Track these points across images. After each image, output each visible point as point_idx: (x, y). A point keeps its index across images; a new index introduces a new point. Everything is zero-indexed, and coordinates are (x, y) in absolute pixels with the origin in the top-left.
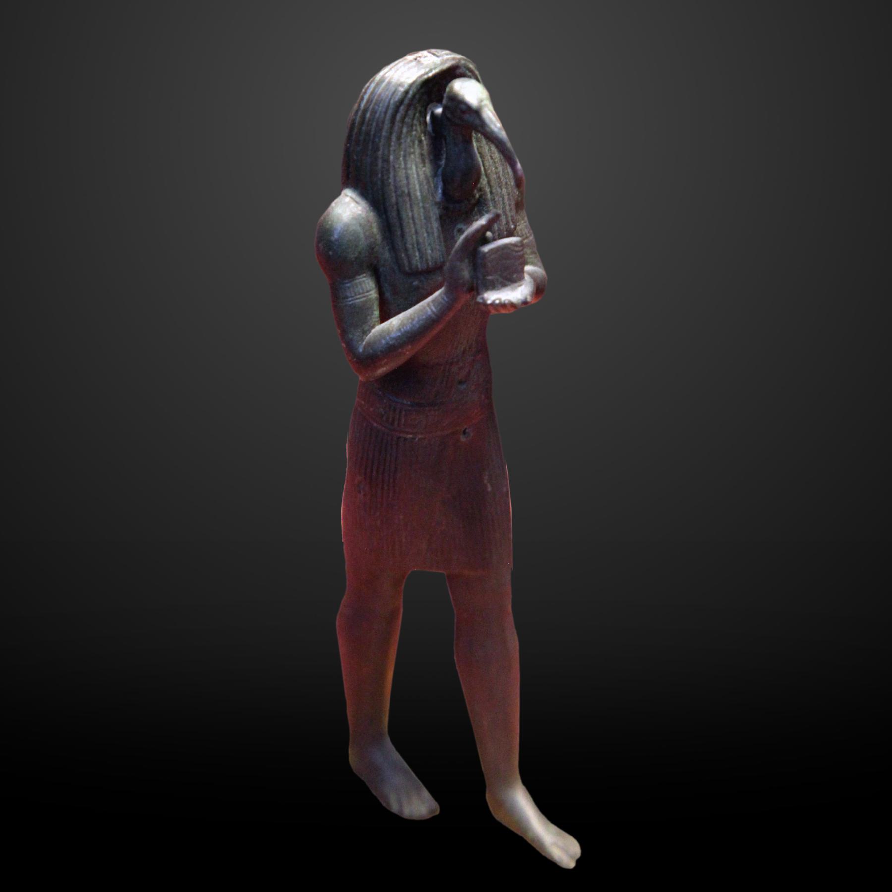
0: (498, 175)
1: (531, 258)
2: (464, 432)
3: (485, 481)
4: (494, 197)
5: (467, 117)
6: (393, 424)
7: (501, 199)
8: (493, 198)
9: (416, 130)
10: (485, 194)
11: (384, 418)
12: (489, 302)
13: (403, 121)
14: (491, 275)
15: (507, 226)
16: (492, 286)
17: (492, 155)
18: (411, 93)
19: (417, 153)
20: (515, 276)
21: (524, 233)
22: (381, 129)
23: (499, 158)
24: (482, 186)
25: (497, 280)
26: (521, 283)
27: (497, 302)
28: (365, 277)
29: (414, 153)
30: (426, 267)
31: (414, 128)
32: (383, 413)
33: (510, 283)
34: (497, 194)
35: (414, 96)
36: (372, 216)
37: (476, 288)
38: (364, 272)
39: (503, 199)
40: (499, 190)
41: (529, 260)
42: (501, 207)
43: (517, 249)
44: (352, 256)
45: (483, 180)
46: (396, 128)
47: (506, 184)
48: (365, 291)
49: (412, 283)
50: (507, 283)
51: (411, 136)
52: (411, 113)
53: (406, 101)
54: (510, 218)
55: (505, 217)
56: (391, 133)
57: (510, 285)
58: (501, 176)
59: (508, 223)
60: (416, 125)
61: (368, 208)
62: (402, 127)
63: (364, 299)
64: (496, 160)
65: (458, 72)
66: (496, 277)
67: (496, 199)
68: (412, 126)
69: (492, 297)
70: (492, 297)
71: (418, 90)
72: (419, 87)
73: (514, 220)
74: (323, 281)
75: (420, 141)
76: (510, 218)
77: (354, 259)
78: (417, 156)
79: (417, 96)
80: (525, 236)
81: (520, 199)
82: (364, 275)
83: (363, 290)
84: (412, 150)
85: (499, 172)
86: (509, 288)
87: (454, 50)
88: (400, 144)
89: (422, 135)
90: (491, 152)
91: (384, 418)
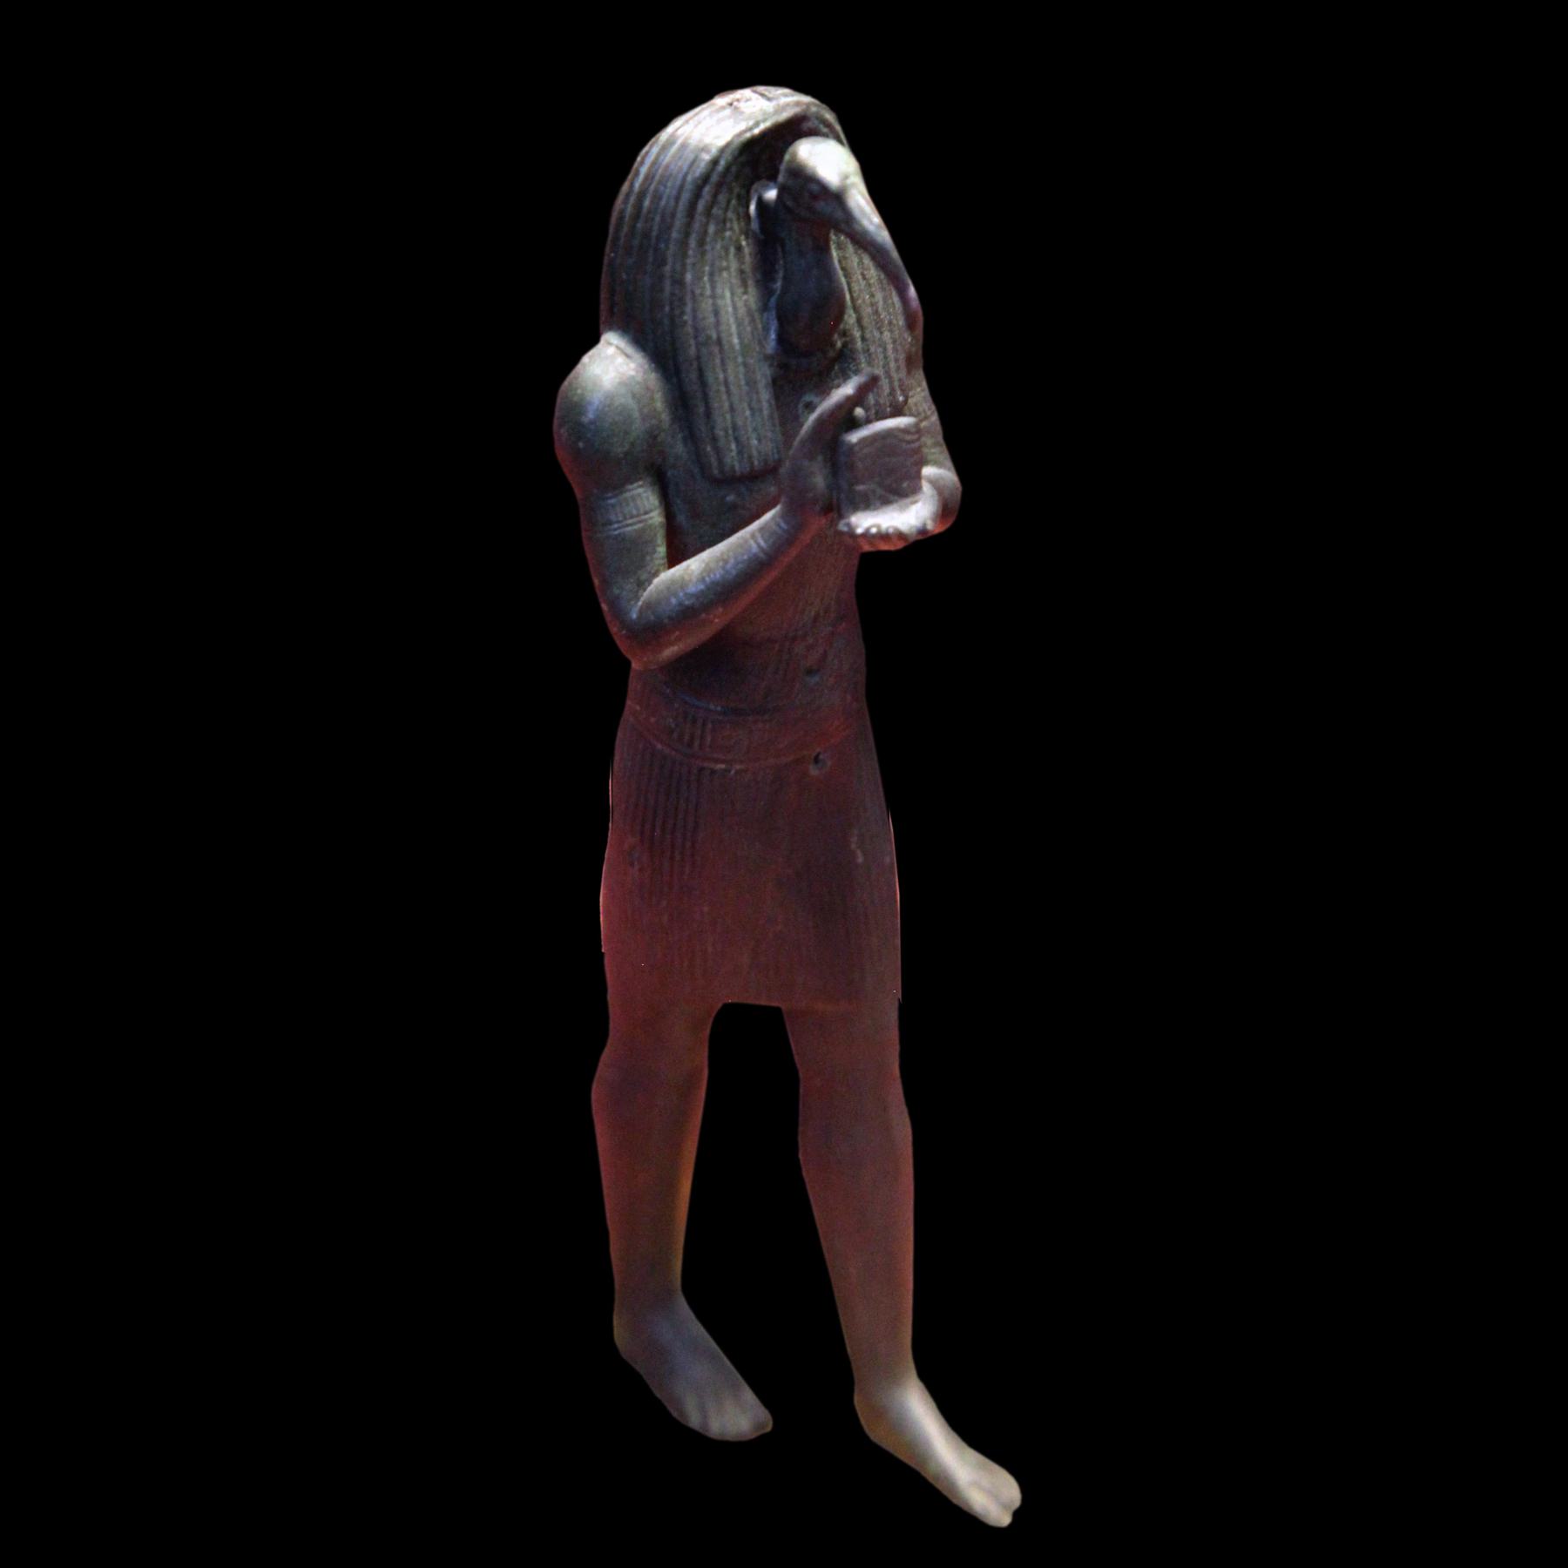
1: (934, 453)
2: (816, 760)
3: (853, 846)
4: (868, 345)
5: (820, 206)
6: (690, 745)
7: (880, 350)
8: (866, 348)
9: (731, 229)
10: (853, 340)
11: (675, 735)
13: (708, 213)
14: (863, 483)
15: (891, 398)
16: (865, 503)
17: (865, 272)
18: (722, 163)
19: (732, 269)
20: (905, 485)
21: (921, 409)
22: (670, 228)
23: (877, 278)
24: (847, 327)
25: (874, 492)
26: (916, 498)
27: (874, 530)
28: (641, 486)
29: (727, 269)
30: (748, 469)
31: (728, 225)
32: (673, 726)
33: (896, 498)
34: (874, 341)
35: (728, 169)
36: (653, 379)
38: (640, 479)
39: (885, 349)
40: (876, 334)
41: (930, 457)
42: (881, 363)
43: (908, 438)
44: (620, 450)
46: (696, 226)
47: (890, 323)
48: (642, 512)
49: (724, 497)
50: (891, 497)
51: (723, 239)
52: (722, 198)
53: (715, 178)
54: (896, 384)
55: (887, 381)
56: (687, 234)
57: (897, 501)
58: (880, 309)
59: (892, 392)
60: (731, 220)
61: (646, 366)
62: (707, 224)
64: (872, 281)
65: (806, 126)
66: (873, 486)
67: (872, 349)
68: (724, 221)
69: (865, 522)
70: (865, 522)
71: (735, 159)
72: (736, 153)
73: (903, 388)
75: (739, 249)
76: (896, 384)
77: (621, 455)
78: (734, 274)
79: (734, 169)
80: (923, 415)
82: (641, 483)
84: (725, 264)
85: (877, 303)
86: (895, 506)
89: (743, 237)
91: (675, 735)
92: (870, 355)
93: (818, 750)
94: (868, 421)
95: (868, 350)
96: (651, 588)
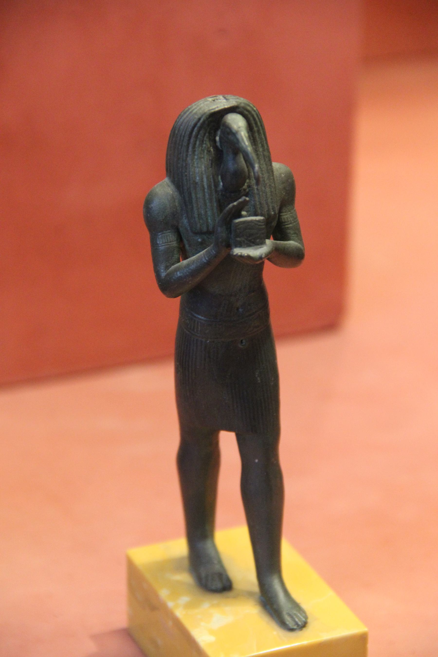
0: (263, 179)
1: (293, 237)
2: (242, 342)
3: (257, 376)
4: (259, 192)
5: (230, 137)
6: (193, 330)
7: (265, 194)
8: (258, 193)
9: (205, 144)
10: (253, 189)
11: (189, 326)
12: (235, 254)
13: (196, 137)
14: (240, 238)
15: (268, 212)
16: (240, 245)
17: (261, 166)
18: (201, 121)
19: (205, 158)
20: (258, 241)
21: (289, 220)
22: (199, 144)
23: (266, 168)
24: (251, 184)
25: (244, 242)
26: (262, 246)
27: (239, 254)
28: (169, 232)
29: (203, 158)
30: (206, 230)
31: (205, 142)
32: (189, 323)
33: (253, 245)
34: (262, 191)
35: (204, 122)
36: (176, 194)
37: (229, 246)
38: (169, 230)
39: (266, 195)
40: (263, 188)
41: (292, 238)
42: (264, 199)
43: (259, 224)
44: (161, 218)
45: (253, 180)
46: (192, 140)
47: (270, 185)
48: (169, 241)
49: (198, 239)
50: (251, 244)
51: (202, 147)
52: (202, 132)
53: (199, 125)
54: (271, 207)
55: (267, 206)
56: (188, 144)
57: (253, 246)
58: (265, 179)
59: (269, 210)
60: (206, 141)
61: (174, 190)
62: (196, 141)
63: (168, 246)
64: (263, 169)
65: (238, 110)
66: (243, 239)
67: (261, 193)
68: (203, 141)
69: (238, 251)
70: (238, 251)
71: (207, 119)
72: (208, 117)
73: (274, 209)
74: (146, 235)
75: (209, 151)
76: (271, 207)
77: (162, 220)
78: (206, 160)
79: (206, 122)
80: (290, 222)
81: (287, 198)
82: (169, 231)
83: (168, 240)
84: (202, 156)
85: (264, 177)
86: (252, 248)
87: (244, 97)
88: (195, 151)
89: (212, 148)
90: (260, 164)
91: (189, 326)
92: (260, 195)
93: (242, 339)
94: (245, 216)
95: (259, 194)
96: (171, 269)
